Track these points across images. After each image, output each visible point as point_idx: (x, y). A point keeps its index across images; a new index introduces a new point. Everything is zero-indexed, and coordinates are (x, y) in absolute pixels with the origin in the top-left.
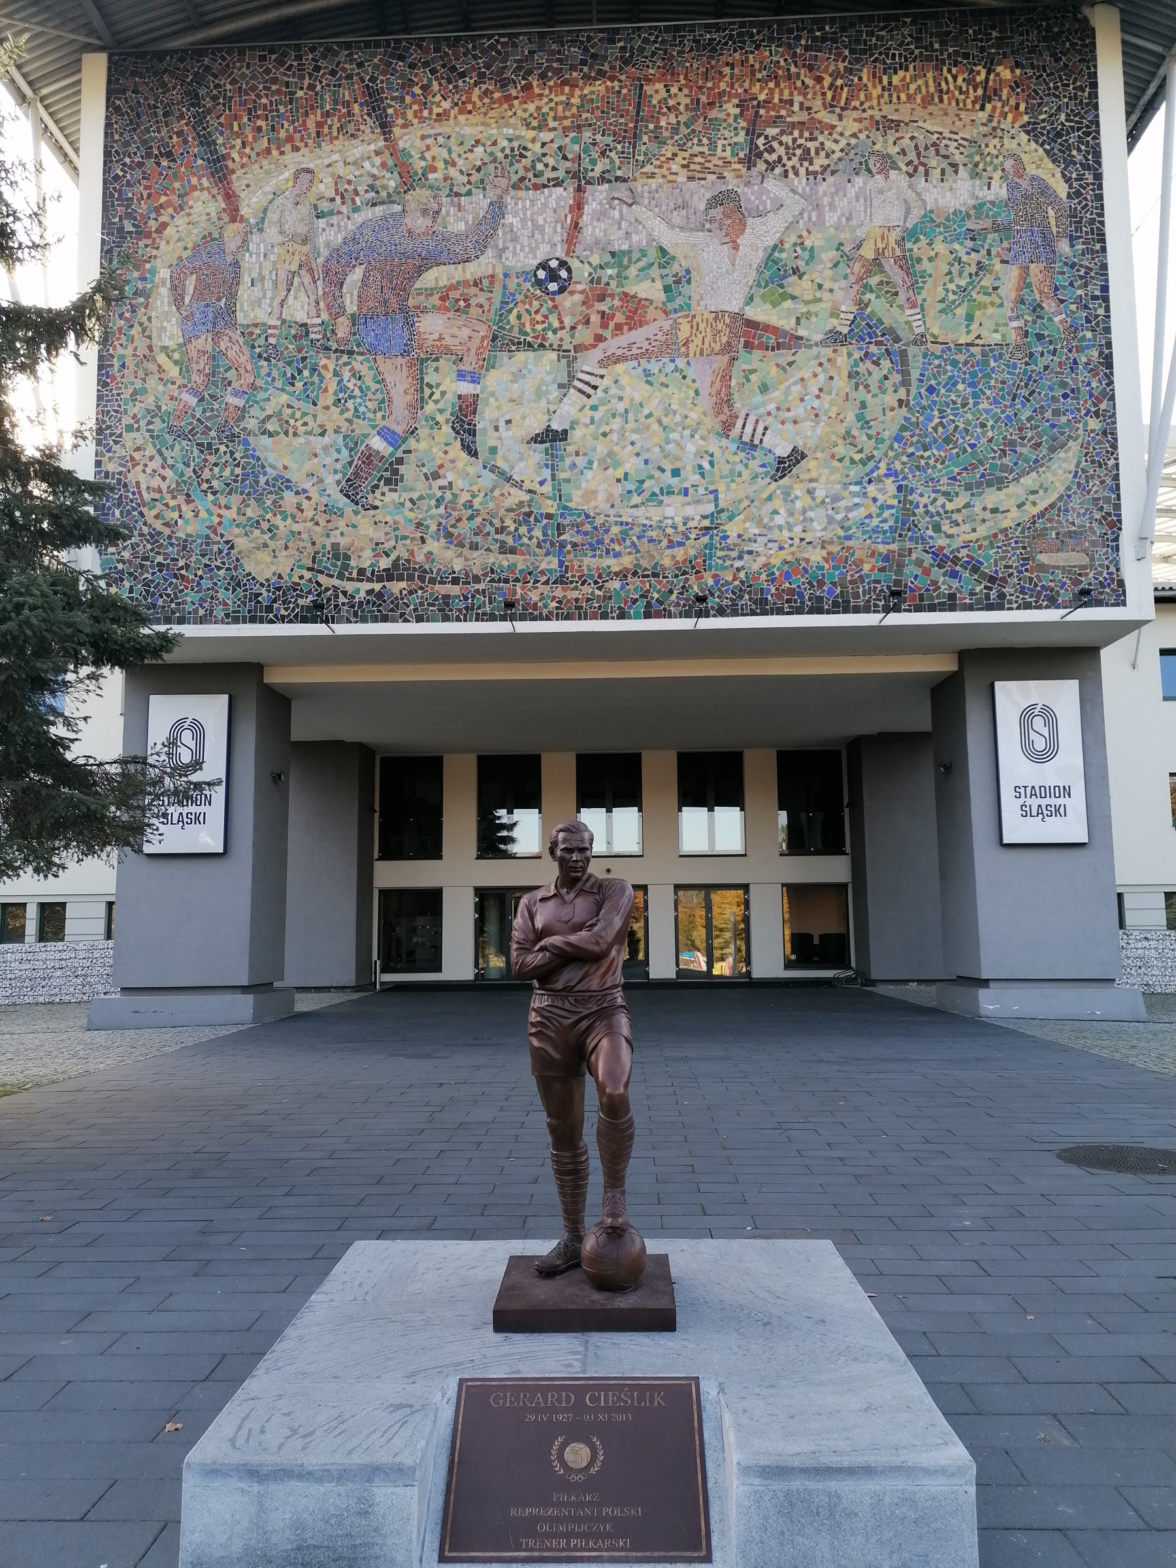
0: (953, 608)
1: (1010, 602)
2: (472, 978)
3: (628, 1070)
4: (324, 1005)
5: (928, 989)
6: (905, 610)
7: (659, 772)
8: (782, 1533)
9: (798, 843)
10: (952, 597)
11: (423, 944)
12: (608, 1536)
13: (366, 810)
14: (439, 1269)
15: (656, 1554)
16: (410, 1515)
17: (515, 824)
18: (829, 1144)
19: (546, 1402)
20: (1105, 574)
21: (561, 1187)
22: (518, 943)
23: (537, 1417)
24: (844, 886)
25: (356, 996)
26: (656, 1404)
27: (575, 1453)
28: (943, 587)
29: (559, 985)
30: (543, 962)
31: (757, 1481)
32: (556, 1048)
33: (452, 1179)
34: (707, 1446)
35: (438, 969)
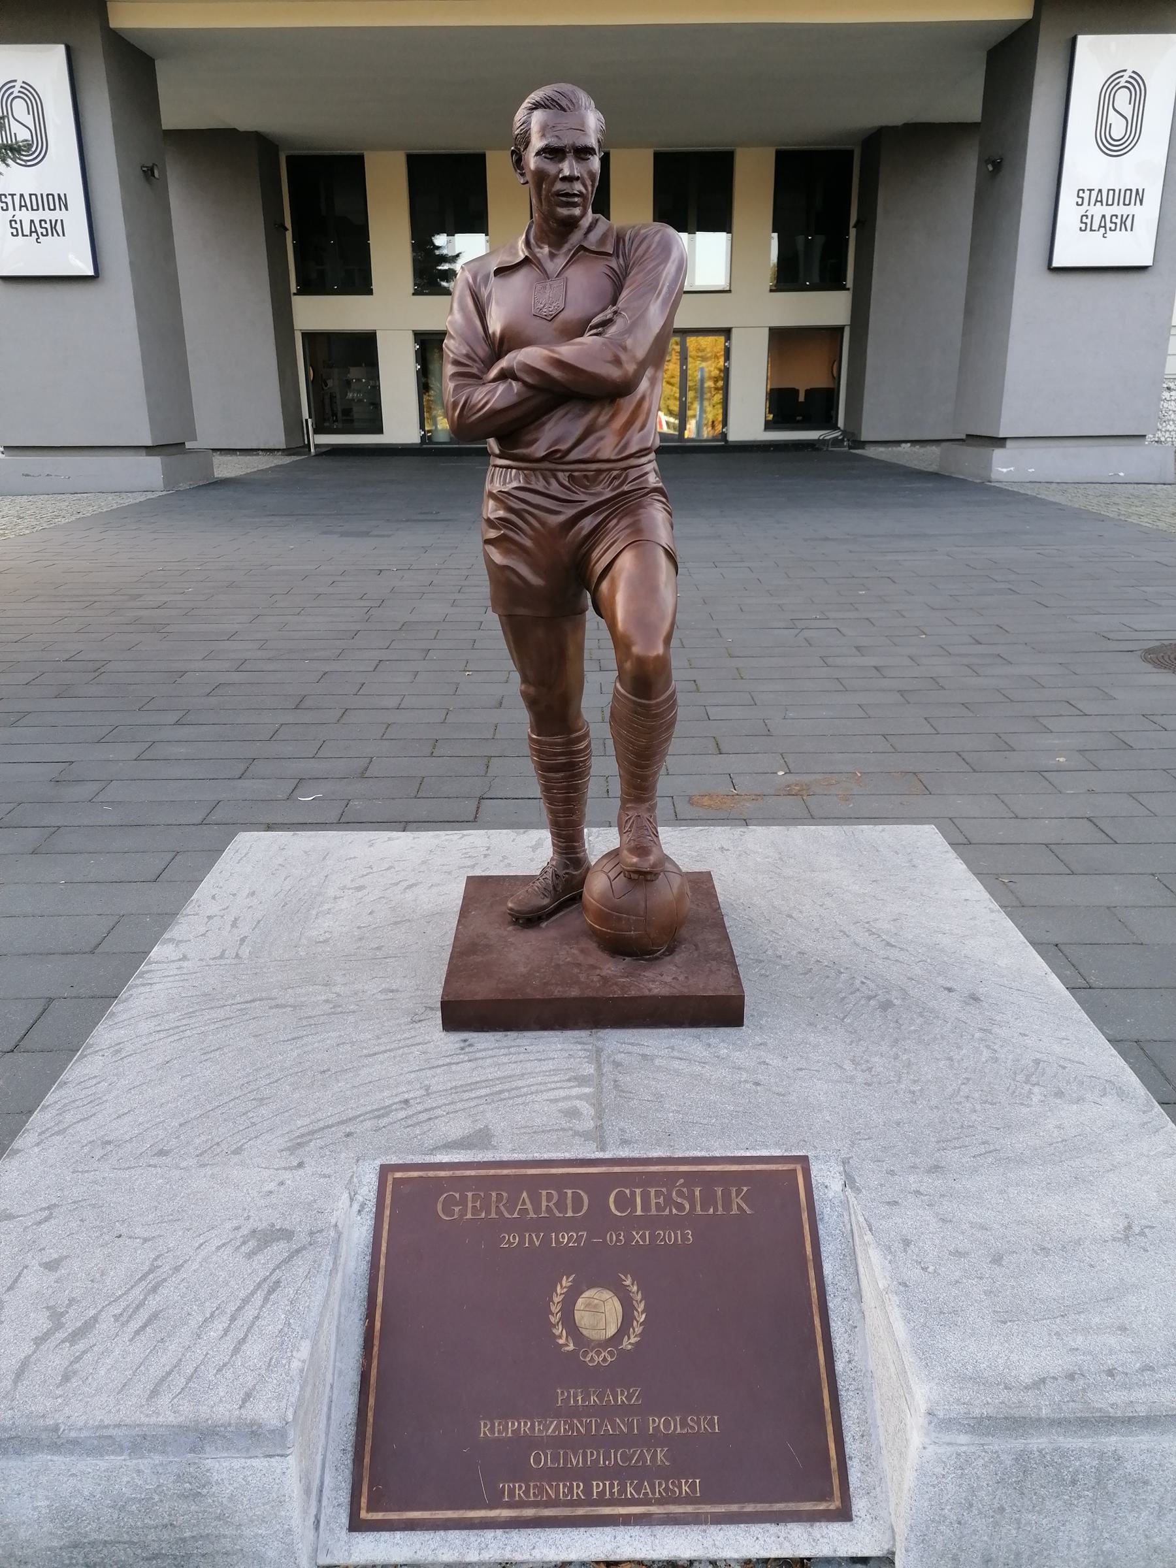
2: (417, 440)
3: (670, 610)
4: (249, 471)
8: (1002, 1509)
9: (789, 276)
11: (360, 401)
12: (664, 1474)
13: (274, 228)
14: (359, 888)
15: (750, 1508)
16: (289, 1487)
17: (458, 256)
18: (857, 648)
19: (537, 1210)
21: (547, 789)
22: (456, 363)
23: (522, 1240)
24: (839, 330)
25: (287, 460)
26: (735, 1211)
27: (591, 1308)
29: (539, 449)
30: (502, 405)
31: (963, 1439)
32: (534, 567)
33: (392, 702)
34: (830, 1289)
35: (379, 430)
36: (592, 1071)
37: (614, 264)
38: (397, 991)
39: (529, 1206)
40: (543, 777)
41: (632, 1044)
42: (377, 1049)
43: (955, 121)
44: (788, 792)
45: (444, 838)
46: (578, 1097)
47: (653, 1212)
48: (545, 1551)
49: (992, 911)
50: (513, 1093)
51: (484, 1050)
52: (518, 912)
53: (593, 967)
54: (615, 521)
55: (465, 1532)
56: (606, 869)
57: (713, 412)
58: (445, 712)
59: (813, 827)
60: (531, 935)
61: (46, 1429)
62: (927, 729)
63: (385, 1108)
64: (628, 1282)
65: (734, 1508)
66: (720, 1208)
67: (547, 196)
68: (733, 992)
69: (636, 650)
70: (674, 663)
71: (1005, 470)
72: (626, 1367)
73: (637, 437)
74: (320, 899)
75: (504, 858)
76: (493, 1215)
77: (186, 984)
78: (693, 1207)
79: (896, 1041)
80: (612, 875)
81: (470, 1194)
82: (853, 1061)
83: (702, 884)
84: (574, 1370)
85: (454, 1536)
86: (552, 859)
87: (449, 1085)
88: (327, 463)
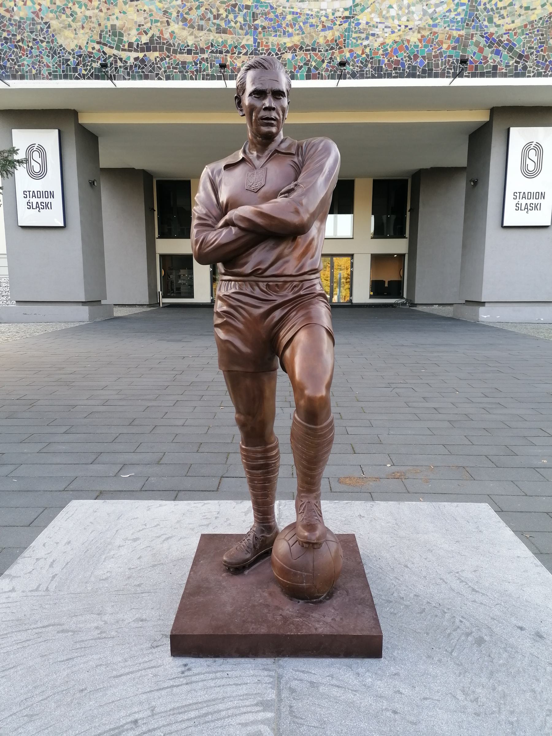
0: (494, 75)
1: (529, 72)
5: (444, 308)
6: (466, 76)
10: (495, 68)
11: (184, 284)
13: (149, 210)
14: (135, 540)
18: (424, 398)
22: (200, 218)
24: (403, 255)
25: (149, 309)
28: (490, 61)
29: (248, 269)
32: (244, 341)
33: (180, 422)
35: (192, 296)
36: (274, 696)
37: (296, 160)
38: (146, 620)
40: (248, 472)
41: (303, 672)
42: (122, 671)
44: (394, 476)
45: (193, 505)
46: (263, 722)
49: (537, 566)
50: (216, 716)
51: (198, 674)
52: (229, 563)
53: (278, 608)
54: (294, 313)
56: (287, 538)
57: (345, 292)
58: (207, 428)
59: (414, 503)
60: (238, 580)
62: (467, 442)
63: (118, 728)
67: (255, 119)
68: (374, 633)
69: (307, 392)
70: (333, 404)
71: (485, 317)
73: (309, 261)
74: (110, 547)
75: (228, 519)
77: (8, 611)
79: (492, 673)
80: (291, 542)
82: (463, 691)
83: (348, 542)
86: (254, 526)
87: (170, 707)
88: (167, 310)
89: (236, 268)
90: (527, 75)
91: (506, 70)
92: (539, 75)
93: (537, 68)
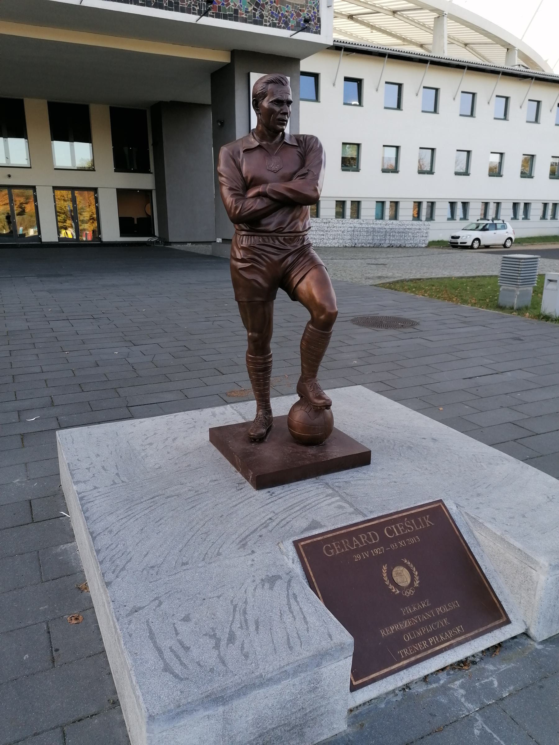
0: (236, 19)
1: (266, 21)
5: (197, 246)
6: (211, 16)
7: (36, 114)
10: (236, 11)
12: (451, 627)
20: (312, 13)
28: (232, 4)
37: (299, 150)
39: (358, 543)
43: (193, 102)
47: (402, 533)
48: (424, 671)
55: (393, 676)
61: (257, 677)
64: (406, 561)
65: (476, 631)
66: (397, 533)
72: (420, 594)
76: (347, 550)
78: (414, 528)
81: (334, 544)
84: (402, 600)
85: (390, 678)
89: (260, 227)
90: (264, 23)
91: (246, 15)
92: (274, 25)
93: (272, 18)
